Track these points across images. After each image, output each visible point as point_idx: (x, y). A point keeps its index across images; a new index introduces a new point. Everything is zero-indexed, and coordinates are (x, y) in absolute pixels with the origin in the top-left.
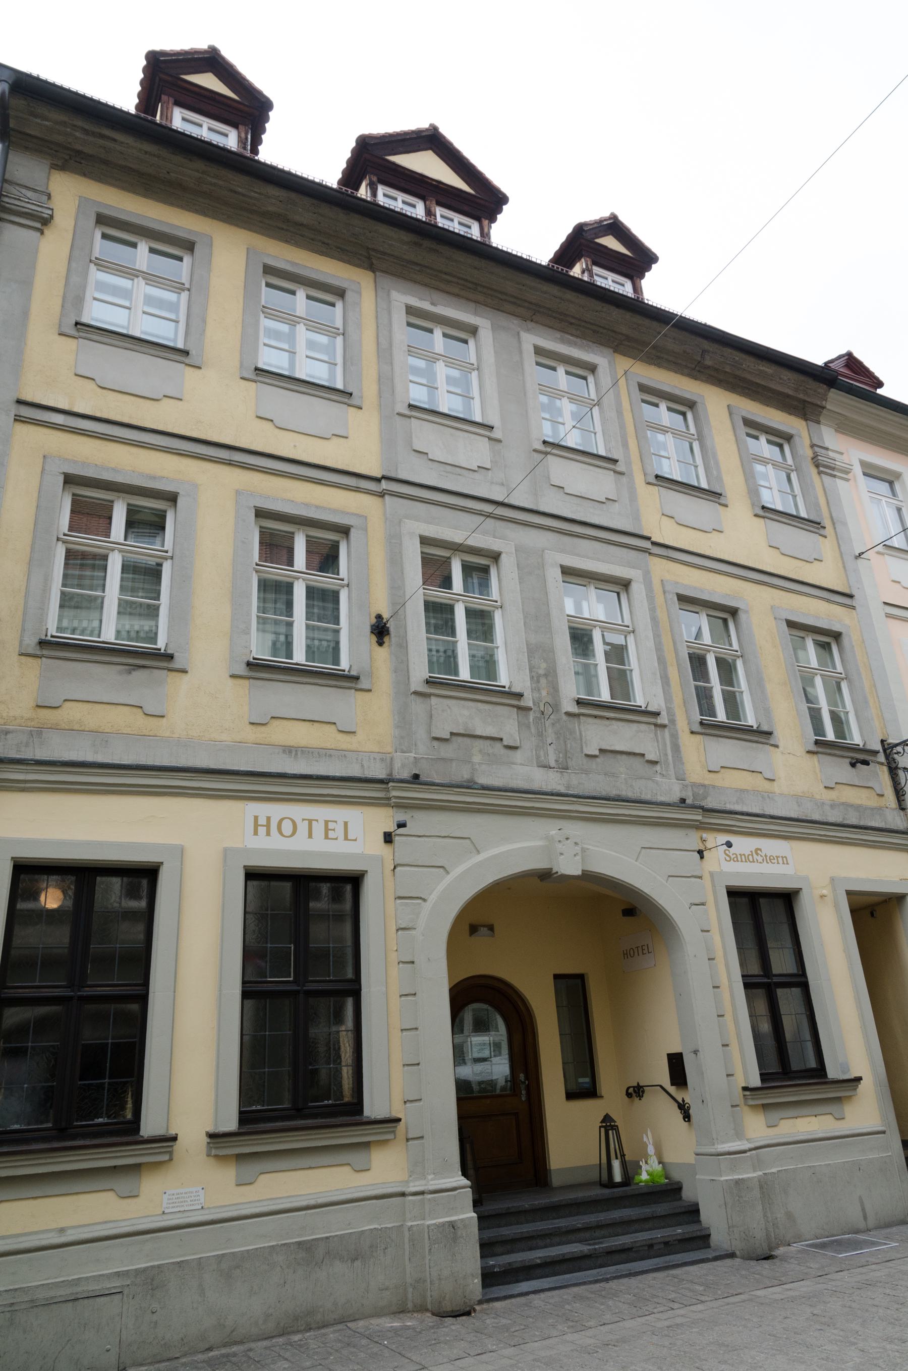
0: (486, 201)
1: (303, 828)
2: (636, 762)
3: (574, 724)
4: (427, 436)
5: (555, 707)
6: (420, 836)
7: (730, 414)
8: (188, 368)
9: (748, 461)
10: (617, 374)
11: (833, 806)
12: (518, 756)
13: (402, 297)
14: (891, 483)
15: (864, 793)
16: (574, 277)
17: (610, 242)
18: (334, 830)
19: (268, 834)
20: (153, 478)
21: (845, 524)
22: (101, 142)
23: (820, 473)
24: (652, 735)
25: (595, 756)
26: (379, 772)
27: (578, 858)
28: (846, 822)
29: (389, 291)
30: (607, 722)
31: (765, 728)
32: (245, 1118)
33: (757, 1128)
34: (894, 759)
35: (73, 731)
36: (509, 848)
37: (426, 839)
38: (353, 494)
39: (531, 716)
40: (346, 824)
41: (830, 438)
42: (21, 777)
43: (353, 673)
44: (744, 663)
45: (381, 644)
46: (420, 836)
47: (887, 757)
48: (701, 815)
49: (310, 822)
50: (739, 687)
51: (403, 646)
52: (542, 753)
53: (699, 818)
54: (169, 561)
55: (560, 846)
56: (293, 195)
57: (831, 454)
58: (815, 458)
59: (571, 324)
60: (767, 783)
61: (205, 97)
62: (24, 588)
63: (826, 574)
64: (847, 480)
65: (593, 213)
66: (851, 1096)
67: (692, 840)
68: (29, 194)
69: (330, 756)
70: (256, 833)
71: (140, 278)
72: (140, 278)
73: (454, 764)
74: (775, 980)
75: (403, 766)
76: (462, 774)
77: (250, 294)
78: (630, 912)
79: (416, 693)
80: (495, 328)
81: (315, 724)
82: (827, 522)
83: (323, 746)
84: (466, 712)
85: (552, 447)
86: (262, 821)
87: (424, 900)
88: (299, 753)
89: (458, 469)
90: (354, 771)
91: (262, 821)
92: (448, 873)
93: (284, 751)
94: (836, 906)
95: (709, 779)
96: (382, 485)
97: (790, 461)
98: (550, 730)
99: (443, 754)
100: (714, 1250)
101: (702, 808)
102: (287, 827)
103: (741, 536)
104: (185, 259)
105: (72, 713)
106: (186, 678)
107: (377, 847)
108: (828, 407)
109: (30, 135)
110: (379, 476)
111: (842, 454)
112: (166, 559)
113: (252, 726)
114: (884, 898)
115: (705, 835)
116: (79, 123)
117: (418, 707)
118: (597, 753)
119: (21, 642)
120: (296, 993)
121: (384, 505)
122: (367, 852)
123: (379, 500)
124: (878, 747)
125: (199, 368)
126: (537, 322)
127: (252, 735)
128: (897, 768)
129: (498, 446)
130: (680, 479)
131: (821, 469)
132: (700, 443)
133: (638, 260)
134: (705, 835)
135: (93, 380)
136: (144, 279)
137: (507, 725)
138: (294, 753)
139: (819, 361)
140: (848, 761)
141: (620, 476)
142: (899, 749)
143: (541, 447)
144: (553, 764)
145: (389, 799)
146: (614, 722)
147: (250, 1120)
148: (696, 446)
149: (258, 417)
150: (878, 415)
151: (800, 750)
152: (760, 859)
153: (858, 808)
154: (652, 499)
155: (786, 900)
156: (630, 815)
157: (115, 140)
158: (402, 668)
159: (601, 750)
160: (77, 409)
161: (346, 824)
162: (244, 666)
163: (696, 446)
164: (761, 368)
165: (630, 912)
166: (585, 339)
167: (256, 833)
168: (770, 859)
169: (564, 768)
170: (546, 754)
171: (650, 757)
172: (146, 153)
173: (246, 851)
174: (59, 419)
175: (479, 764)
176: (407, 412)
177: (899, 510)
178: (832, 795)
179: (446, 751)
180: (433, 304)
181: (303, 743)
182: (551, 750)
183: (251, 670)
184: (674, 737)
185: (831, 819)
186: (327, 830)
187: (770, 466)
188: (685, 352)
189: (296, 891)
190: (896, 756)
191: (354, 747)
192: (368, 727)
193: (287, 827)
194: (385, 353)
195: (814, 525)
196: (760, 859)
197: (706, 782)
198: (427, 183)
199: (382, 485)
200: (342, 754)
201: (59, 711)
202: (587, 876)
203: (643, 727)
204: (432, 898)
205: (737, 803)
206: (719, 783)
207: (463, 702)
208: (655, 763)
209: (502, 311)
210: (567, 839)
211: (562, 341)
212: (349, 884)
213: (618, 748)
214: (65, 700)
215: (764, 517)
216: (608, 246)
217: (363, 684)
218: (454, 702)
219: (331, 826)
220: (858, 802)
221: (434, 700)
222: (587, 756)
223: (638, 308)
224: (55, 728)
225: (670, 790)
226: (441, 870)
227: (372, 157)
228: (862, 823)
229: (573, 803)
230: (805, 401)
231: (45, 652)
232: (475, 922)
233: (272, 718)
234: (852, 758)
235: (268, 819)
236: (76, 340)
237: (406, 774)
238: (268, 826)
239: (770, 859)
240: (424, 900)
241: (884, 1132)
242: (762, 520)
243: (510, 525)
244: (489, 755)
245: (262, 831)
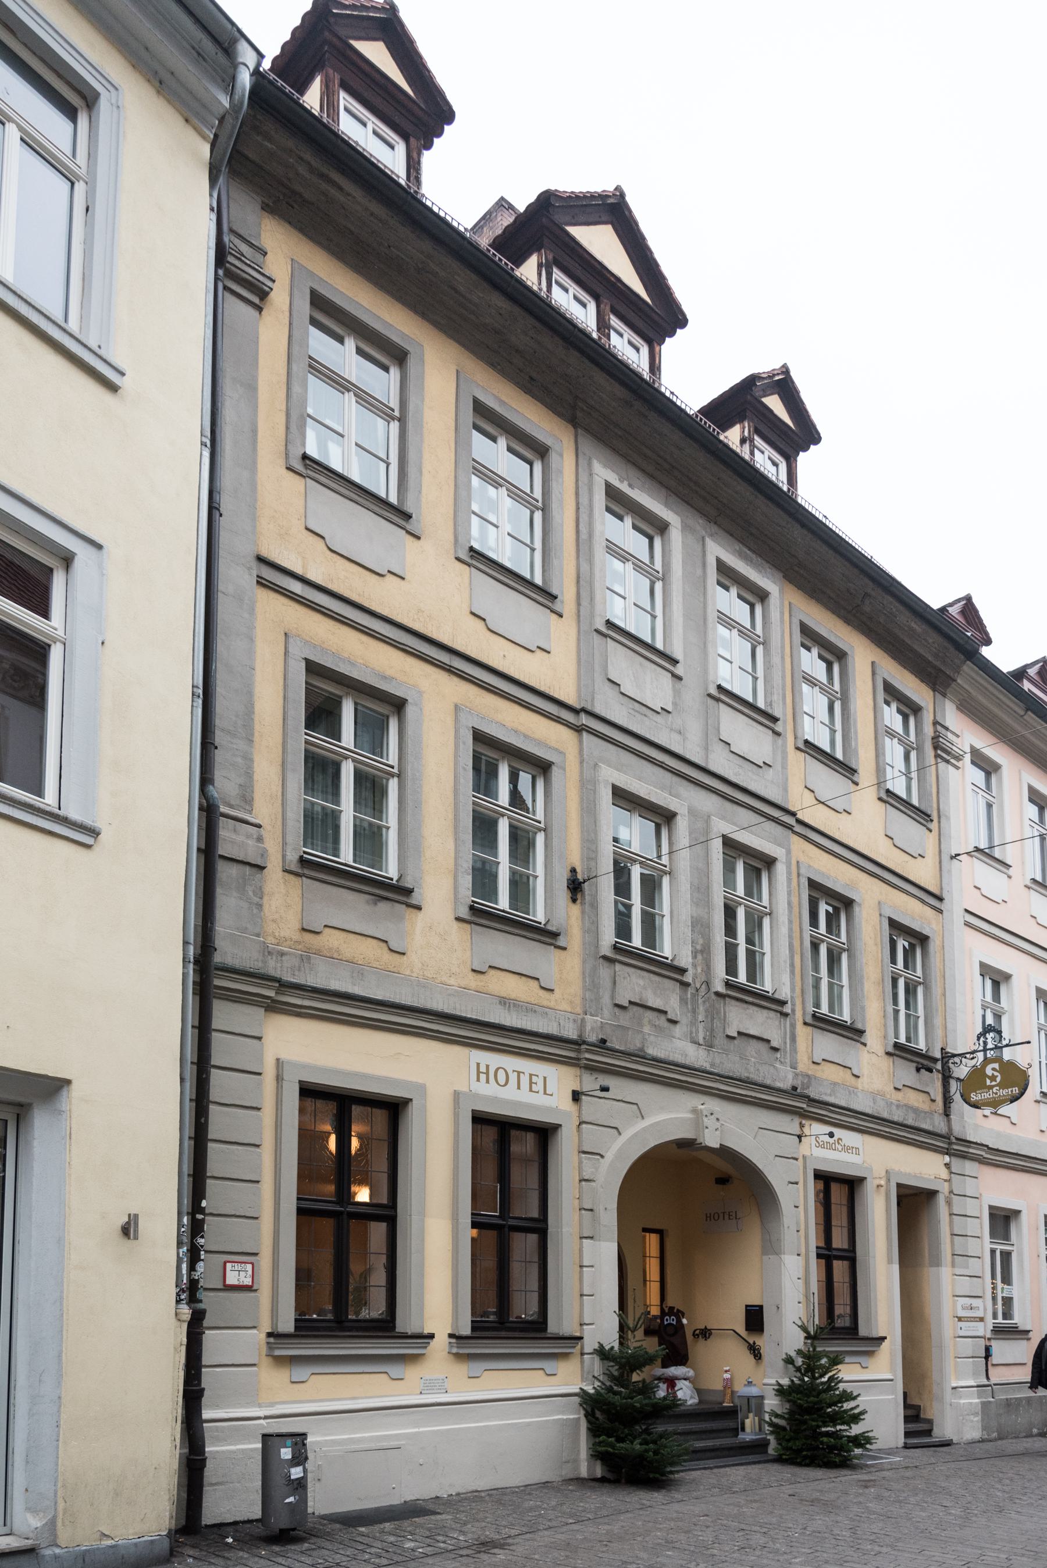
0: (659, 316)
1: (513, 1077)
2: (762, 1047)
3: (720, 1003)
4: (621, 663)
5: (708, 984)
7: (874, 673)
8: (408, 537)
9: (882, 732)
10: (691, 547)
12: (678, 1030)
13: (605, 473)
14: (988, 774)
15: (922, 1097)
16: (726, 446)
17: (774, 403)
19: (488, 1082)
20: (384, 678)
21: (948, 818)
22: (324, 186)
23: (937, 756)
24: (777, 1023)
25: (734, 1038)
26: (571, 1033)
27: (718, 1132)
28: (905, 1122)
29: (590, 459)
30: (745, 1006)
31: (859, 1026)
32: (475, 1326)
34: (949, 1068)
35: (333, 957)
36: (662, 1117)
38: (553, 724)
39: (690, 990)
40: (545, 1078)
41: (953, 718)
42: (299, 1002)
43: (554, 929)
44: (849, 957)
45: (574, 901)
47: (945, 1065)
48: (802, 1105)
49: (519, 1073)
50: (661, 909)
51: (595, 906)
52: (694, 1030)
54: (396, 779)
55: (705, 1119)
56: (517, 310)
57: (950, 735)
58: (936, 738)
59: (751, 534)
60: (853, 1078)
61: (377, 83)
62: (280, 794)
63: (923, 873)
64: (957, 768)
65: (764, 365)
67: (791, 1124)
68: (244, 248)
69: (535, 1011)
70: (478, 1080)
71: (504, 488)
72: (504, 488)
74: (835, 1253)
75: (592, 1029)
76: (633, 1043)
77: (461, 445)
78: (723, 1180)
79: (605, 958)
80: (685, 528)
81: (523, 978)
82: (935, 817)
83: (529, 1000)
84: (641, 982)
85: (724, 695)
86: (483, 1069)
87: (602, 1156)
89: (644, 708)
92: (620, 1134)
95: (812, 1070)
96: (578, 718)
97: (912, 737)
98: (701, 1008)
99: (622, 1023)
101: (808, 1097)
103: (865, 824)
104: (392, 370)
105: (331, 940)
106: (421, 915)
107: (565, 1103)
108: (959, 681)
109: (247, 158)
110: (578, 707)
111: (958, 736)
112: (392, 775)
114: (911, 1192)
115: (804, 1122)
116: (308, 156)
117: (605, 972)
118: (735, 1035)
119: (284, 857)
121: (581, 742)
123: (576, 734)
124: (938, 1055)
125: (418, 538)
126: (719, 526)
127: (473, 981)
128: (950, 1077)
129: (678, 685)
130: (508, 564)
131: (939, 752)
132: (842, 705)
133: (797, 435)
134: (804, 1122)
135: (323, 538)
136: (355, 395)
137: (665, 996)
139: (935, 603)
140: (915, 1065)
141: (776, 737)
142: (957, 1060)
143: (713, 691)
144: (701, 1041)
145: (579, 1059)
146: (750, 1007)
148: (837, 706)
149: (472, 613)
150: (986, 689)
151: (881, 1052)
152: (840, 1148)
153: (916, 1110)
154: (798, 763)
155: (852, 1184)
156: (755, 1098)
157: (341, 189)
158: (593, 930)
159: (739, 1033)
160: (312, 576)
161: (545, 1078)
162: (467, 909)
163: (538, 516)
164: (913, 625)
165: (723, 1180)
166: (761, 556)
167: (478, 1080)
168: (847, 1149)
169: (709, 1045)
170: (697, 1031)
171: (774, 1044)
172: (372, 214)
173: (477, 1096)
174: (297, 587)
176: (604, 629)
177: (989, 806)
178: (899, 1096)
179: (624, 1019)
180: (630, 486)
182: (701, 1026)
183: (474, 914)
184: (793, 1026)
185: (896, 1119)
186: (531, 1083)
187: (503, 491)
188: (848, 591)
190: (951, 1065)
191: (552, 1004)
192: (559, 988)
194: (583, 544)
195: (922, 816)
196: (840, 1148)
197: (810, 1073)
198: (602, 275)
199: (578, 718)
201: (318, 938)
202: (725, 1152)
203: (772, 1014)
204: (609, 1156)
206: (819, 1074)
207: (639, 971)
208: (776, 1050)
209: (692, 506)
211: (667, 505)
212: (544, 1134)
213: (752, 1032)
214: (326, 926)
215: (469, 565)
216: (771, 408)
217: (561, 942)
218: (632, 970)
220: (916, 1104)
221: (618, 967)
222: (728, 1037)
223: (784, 503)
224: (318, 953)
225: (784, 1078)
227: (543, 225)
228: (917, 1125)
229: (716, 1081)
230: (940, 670)
231: (306, 872)
233: (490, 967)
234: (918, 1063)
235: (487, 1066)
236: (303, 480)
237: (592, 1038)
238: (487, 1073)
239: (847, 1149)
240: (602, 1156)
241: (892, 1380)
242: (883, 805)
243: (685, 783)
245: (483, 1077)
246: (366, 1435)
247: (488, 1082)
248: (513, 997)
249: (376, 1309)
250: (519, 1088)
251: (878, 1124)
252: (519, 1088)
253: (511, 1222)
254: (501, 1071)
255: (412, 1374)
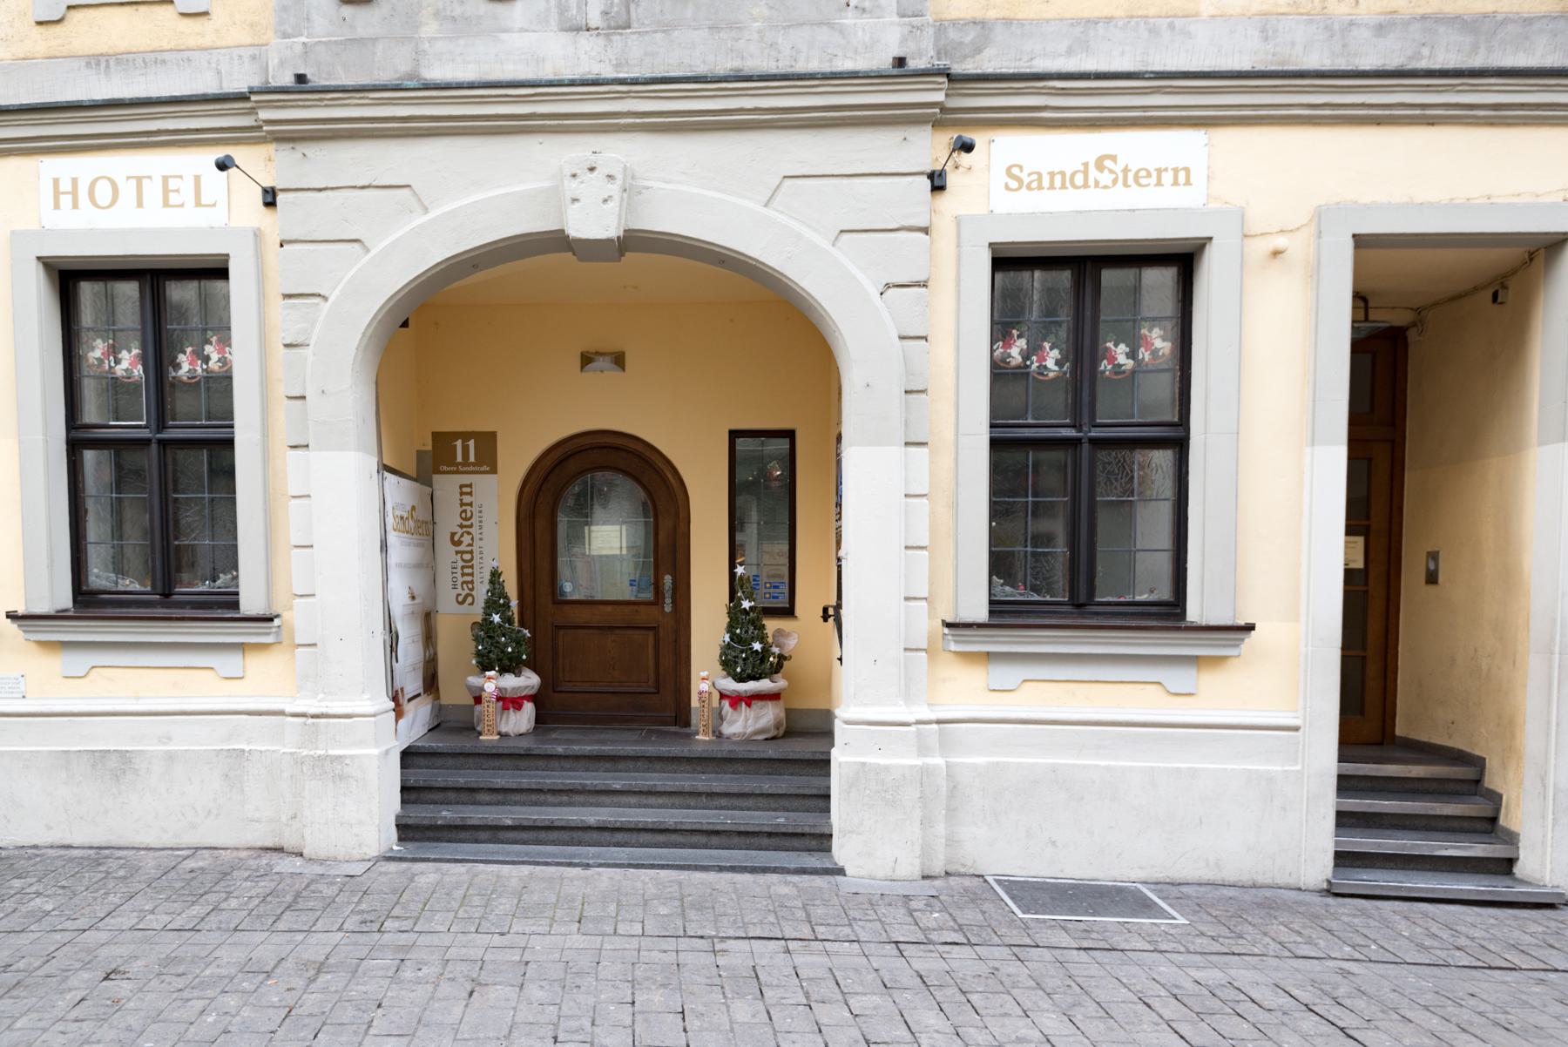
1: (128, 190)
6: (320, 190)
11: (1381, 29)
18: (177, 191)
19: (75, 206)
32: (997, 607)
33: (968, 689)
36: (474, 196)
37: (330, 193)
40: (197, 179)
46: (320, 190)
49: (139, 180)
53: (939, 97)
55: (574, 184)
66: (1226, 657)
69: (164, 62)
70: (57, 206)
73: (380, 47)
75: (282, 63)
76: (389, 65)
83: (156, 45)
86: (65, 186)
87: (325, 298)
88: (112, 63)
90: (205, 84)
91: (65, 186)
93: (88, 64)
94: (1315, 272)
99: (361, 32)
100: (1523, 882)
102: (103, 192)
113: (41, 29)
120: (1074, 443)
122: (233, 224)
127: (41, 42)
138: (103, 65)
147: (1003, 613)
167: (57, 206)
168: (1137, 178)
175: (432, 40)
181: (122, 46)
186: (166, 191)
189: (1078, 286)
191: (207, 41)
193: (103, 192)
200: (183, 55)
202: (633, 242)
205: (1070, 52)
210: (592, 169)
219: (173, 184)
226: (356, 245)
232: (776, 324)
233: (69, 8)
235: (75, 181)
238: (74, 193)
239: (1137, 178)
240: (325, 298)
241: (1296, 729)
244: (454, 19)
245: (66, 200)
246: (1230, 767)
247: (75, 206)
248: (122, 50)
249: (1152, 586)
250: (140, 204)
251: (482, 101)
252: (140, 204)
253: (1095, 433)
254: (100, 184)
255: (1209, 682)
